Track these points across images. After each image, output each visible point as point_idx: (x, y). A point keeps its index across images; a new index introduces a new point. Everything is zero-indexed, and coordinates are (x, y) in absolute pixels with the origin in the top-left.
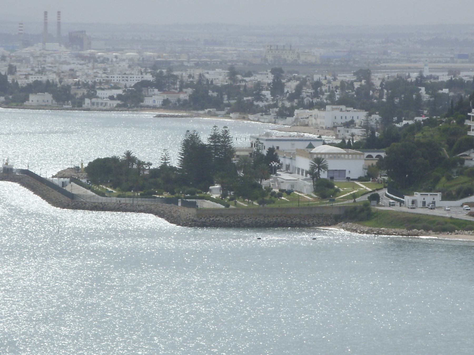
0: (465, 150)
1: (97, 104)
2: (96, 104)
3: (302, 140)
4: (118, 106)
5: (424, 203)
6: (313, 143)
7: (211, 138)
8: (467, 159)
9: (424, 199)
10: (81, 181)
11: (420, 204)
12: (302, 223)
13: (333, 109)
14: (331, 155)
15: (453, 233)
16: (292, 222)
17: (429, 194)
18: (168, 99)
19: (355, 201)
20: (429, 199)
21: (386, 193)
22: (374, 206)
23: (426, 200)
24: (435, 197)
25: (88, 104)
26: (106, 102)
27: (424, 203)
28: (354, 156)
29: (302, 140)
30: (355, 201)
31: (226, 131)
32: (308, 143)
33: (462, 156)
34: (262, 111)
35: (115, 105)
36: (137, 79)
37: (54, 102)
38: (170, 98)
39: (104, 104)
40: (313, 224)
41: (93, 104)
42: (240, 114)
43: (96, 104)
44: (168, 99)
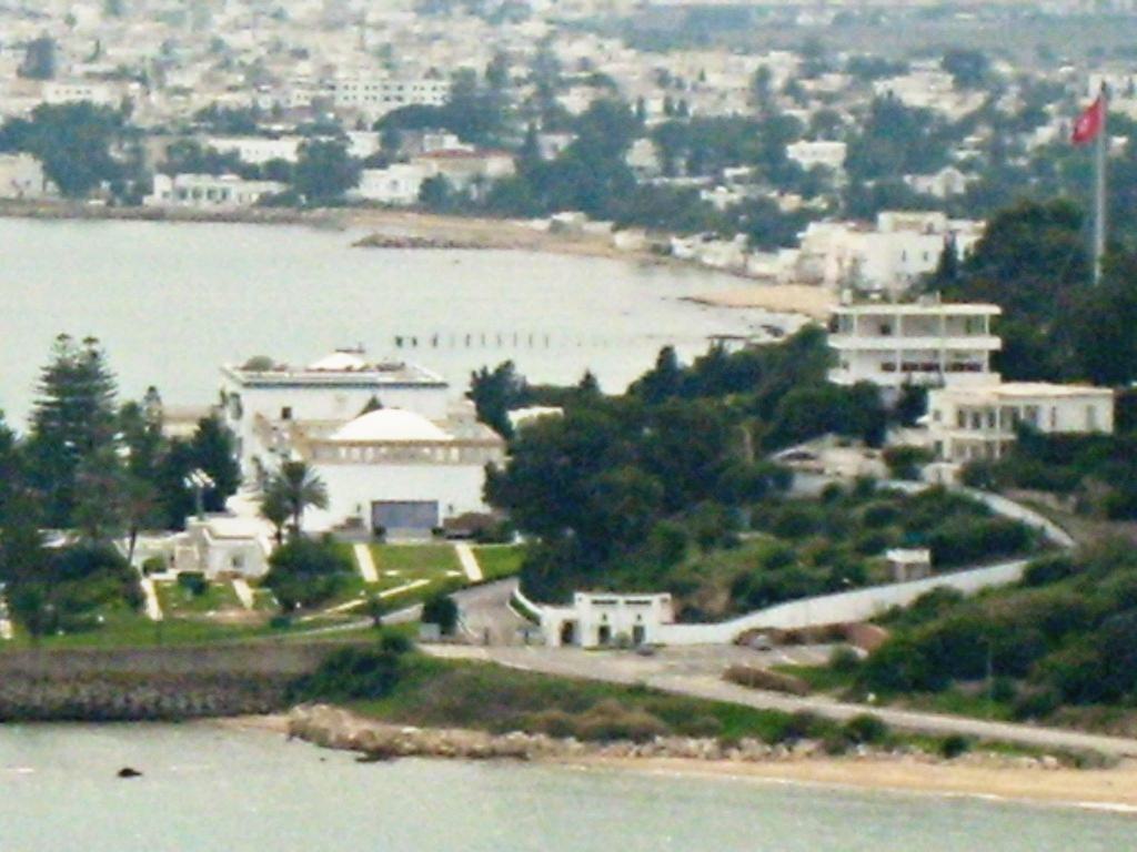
0: (801, 439)
1: (197, 194)
2: (190, 195)
3: (410, 385)
4: (267, 201)
5: (604, 632)
6: (381, 395)
7: (47, 379)
8: (807, 471)
9: (605, 617)
10: (210, 475)
11: (588, 637)
12: (167, 703)
13: (897, 227)
14: (383, 450)
15: (647, 748)
16: (128, 701)
17: (621, 599)
18: (440, 175)
19: (378, 625)
20: (621, 617)
21: (512, 594)
22: (430, 641)
23: (610, 622)
24: (608, 610)
25: (165, 195)
26: (225, 185)
27: (604, 632)
28: (468, 451)
29: (410, 385)
30: (378, 625)
31: (94, 355)
32: (364, 396)
33: (791, 457)
34: (715, 226)
35: (255, 197)
36: (366, 93)
37: (51, 185)
38: (447, 173)
39: (219, 196)
40: (205, 707)
41: (182, 194)
42: (647, 234)
43: (190, 195)
44: (440, 175)
